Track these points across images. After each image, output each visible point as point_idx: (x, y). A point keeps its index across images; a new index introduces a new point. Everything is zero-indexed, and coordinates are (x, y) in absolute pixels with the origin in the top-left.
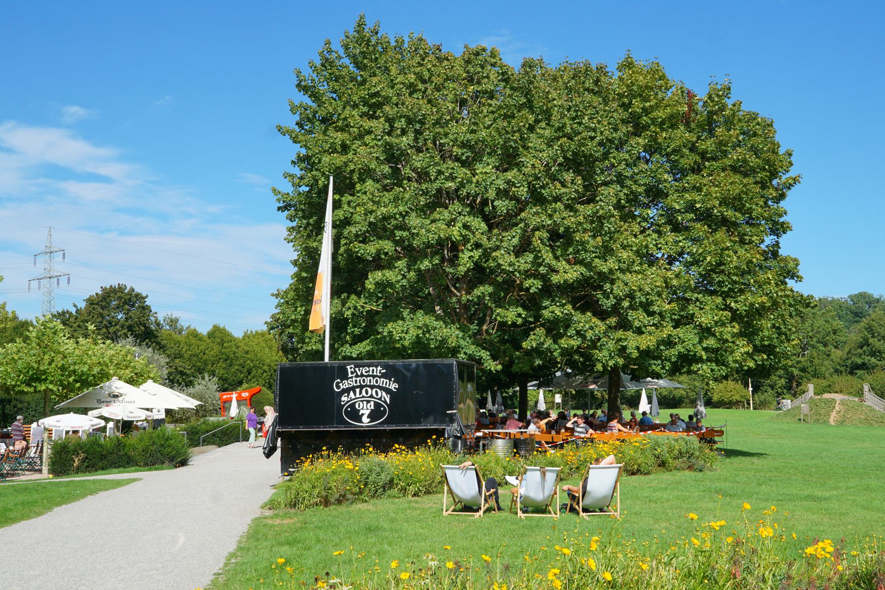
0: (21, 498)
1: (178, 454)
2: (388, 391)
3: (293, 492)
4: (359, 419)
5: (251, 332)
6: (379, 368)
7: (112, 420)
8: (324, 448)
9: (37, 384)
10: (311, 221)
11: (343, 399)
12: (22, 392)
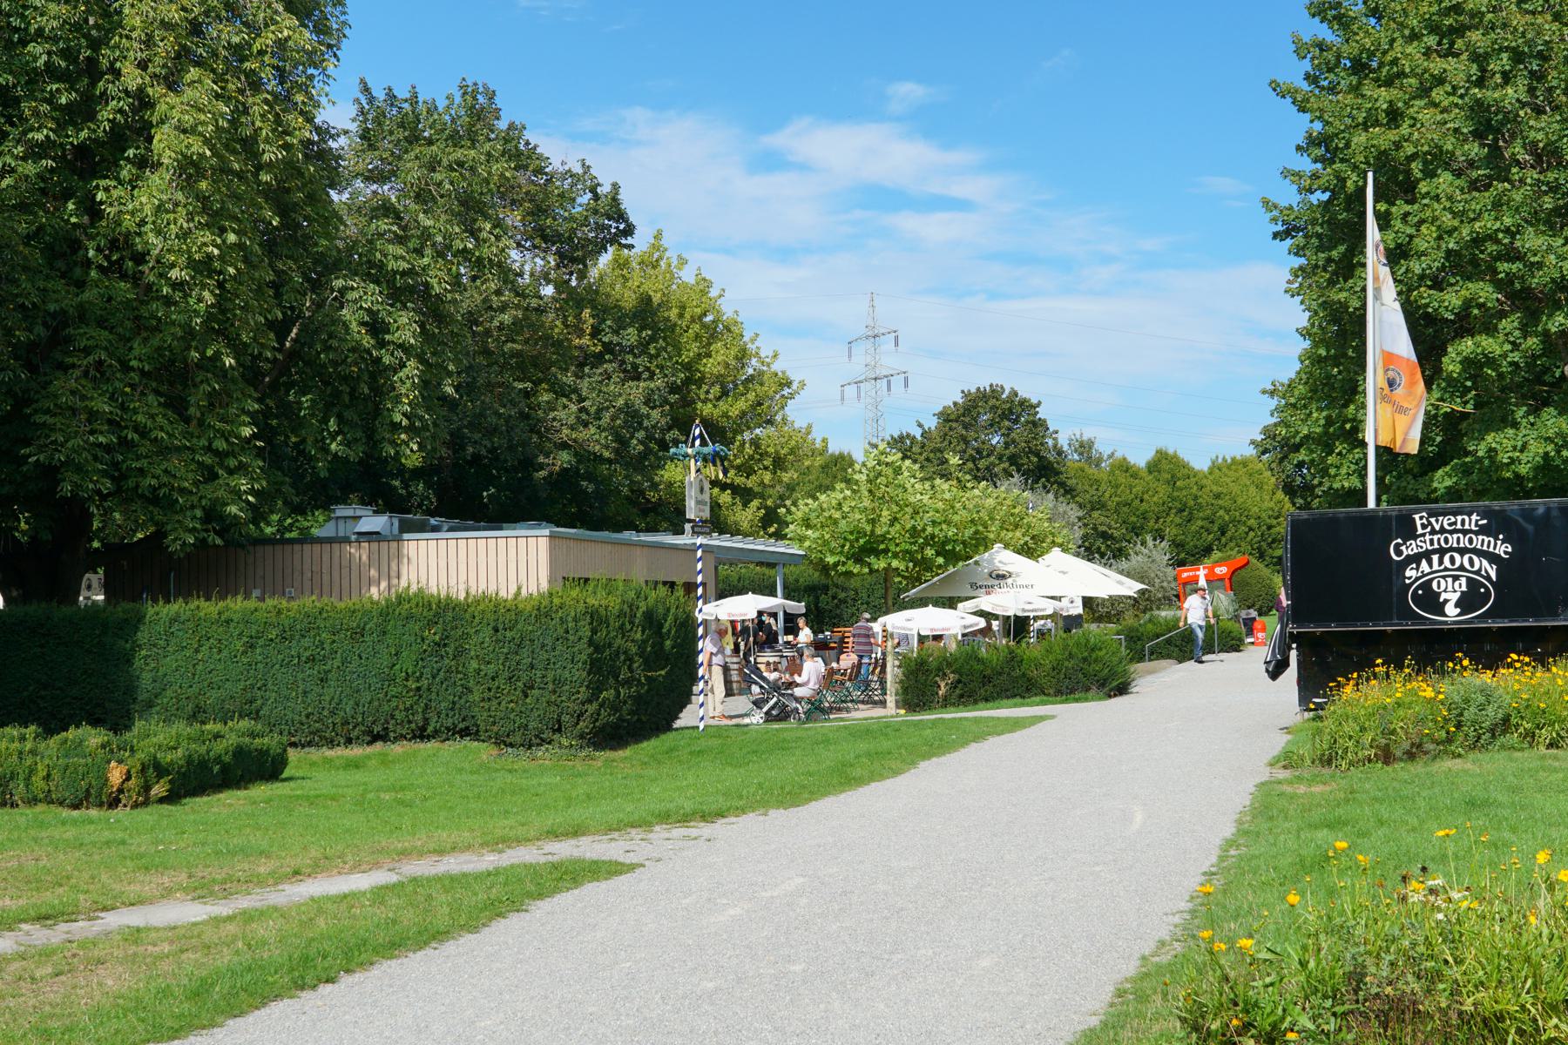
0: (863, 746)
1: (1113, 674)
2: (1493, 558)
3: (1326, 737)
4: (1439, 608)
5: (1224, 459)
6: (1474, 517)
7: (996, 617)
8: (1379, 661)
9: (872, 559)
10: (1334, 254)
11: (1408, 573)
12: (849, 574)
